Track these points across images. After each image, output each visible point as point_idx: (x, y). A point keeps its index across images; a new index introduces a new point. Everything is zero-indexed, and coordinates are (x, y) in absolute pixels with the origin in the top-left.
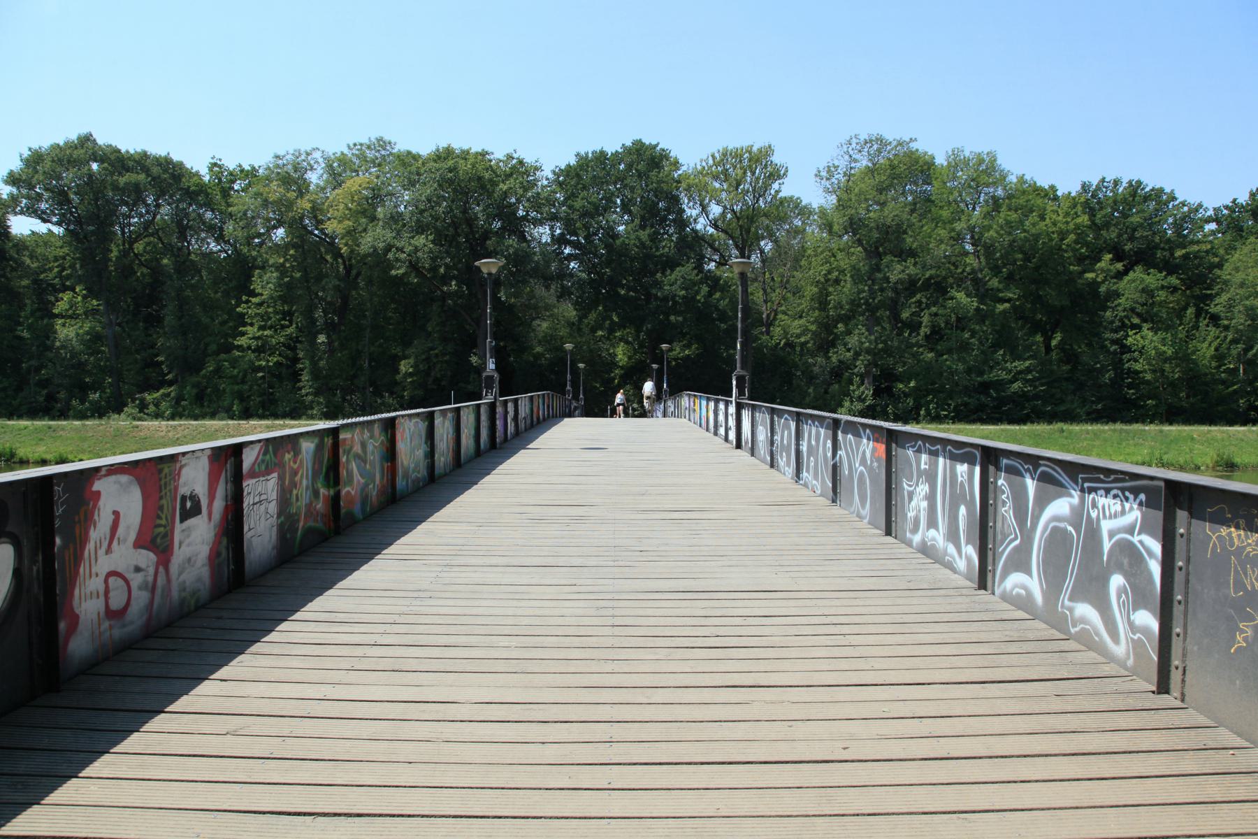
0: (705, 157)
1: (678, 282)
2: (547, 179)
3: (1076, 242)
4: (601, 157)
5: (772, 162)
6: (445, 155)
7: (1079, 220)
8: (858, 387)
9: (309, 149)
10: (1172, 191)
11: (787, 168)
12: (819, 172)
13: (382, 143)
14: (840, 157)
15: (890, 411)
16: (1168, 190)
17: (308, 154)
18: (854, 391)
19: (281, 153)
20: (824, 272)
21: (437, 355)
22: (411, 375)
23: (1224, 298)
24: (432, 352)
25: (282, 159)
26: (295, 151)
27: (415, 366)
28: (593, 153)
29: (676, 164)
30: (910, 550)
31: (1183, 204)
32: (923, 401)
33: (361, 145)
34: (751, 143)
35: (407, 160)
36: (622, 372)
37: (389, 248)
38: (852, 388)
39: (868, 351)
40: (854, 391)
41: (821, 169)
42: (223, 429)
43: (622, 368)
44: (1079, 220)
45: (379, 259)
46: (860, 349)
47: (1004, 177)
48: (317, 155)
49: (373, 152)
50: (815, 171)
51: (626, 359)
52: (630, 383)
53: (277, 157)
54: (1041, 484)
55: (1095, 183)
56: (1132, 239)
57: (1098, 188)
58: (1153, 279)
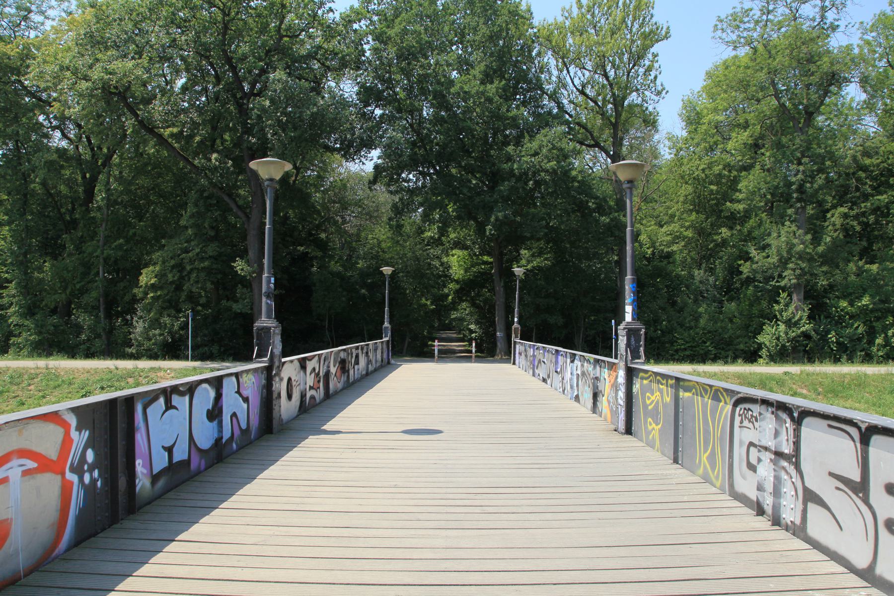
0: (567, 7)
1: (544, 151)
8: (787, 305)
11: (668, 28)
15: (834, 339)
18: (781, 311)
21: (191, 261)
22: (153, 287)
27: (160, 276)
30: (714, 490)
32: (878, 325)
36: (458, 287)
38: (776, 307)
39: (801, 256)
40: (781, 311)
43: (457, 282)
46: (789, 252)
51: (462, 272)
52: (466, 300)
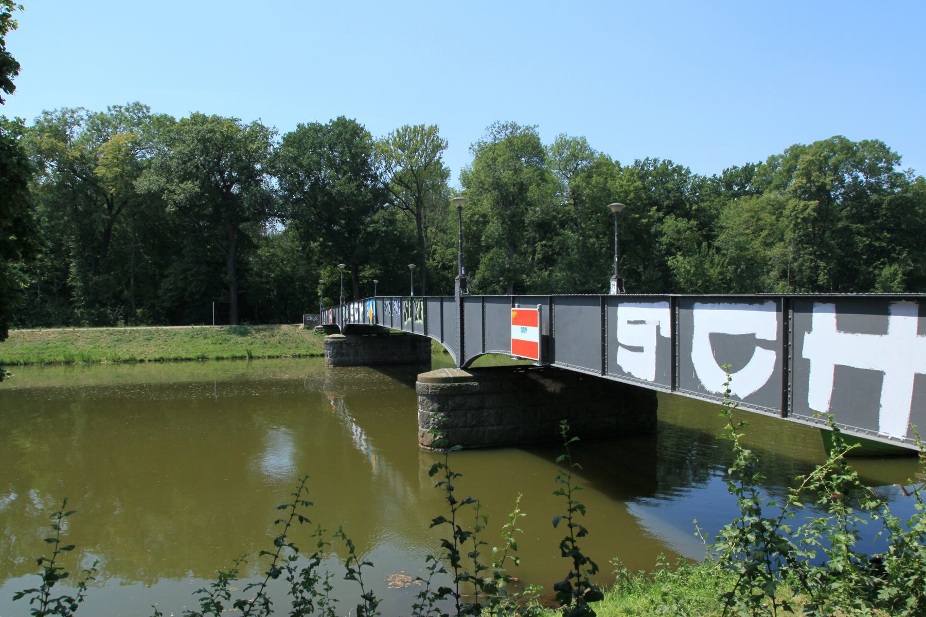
2: (278, 143)
3: (635, 198)
4: (316, 129)
5: (438, 137)
6: (198, 120)
7: (636, 184)
9: (74, 107)
10: (688, 167)
11: (447, 142)
12: (473, 146)
13: (138, 107)
14: (487, 136)
16: (685, 167)
17: (73, 112)
19: (51, 110)
20: (469, 215)
21: (192, 275)
23: (723, 237)
24: (188, 273)
25: (51, 115)
26: (63, 108)
28: (308, 125)
29: (368, 135)
31: (696, 176)
33: (121, 107)
34: (423, 123)
35: (163, 122)
37: (162, 190)
41: (473, 144)
42: (19, 336)
44: (636, 184)
45: (154, 198)
47: (592, 154)
48: (83, 113)
49: (131, 114)
50: (469, 146)
53: (46, 113)
54: (922, 318)
55: (643, 160)
56: (668, 198)
57: (644, 164)
58: (682, 224)
